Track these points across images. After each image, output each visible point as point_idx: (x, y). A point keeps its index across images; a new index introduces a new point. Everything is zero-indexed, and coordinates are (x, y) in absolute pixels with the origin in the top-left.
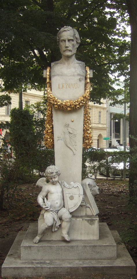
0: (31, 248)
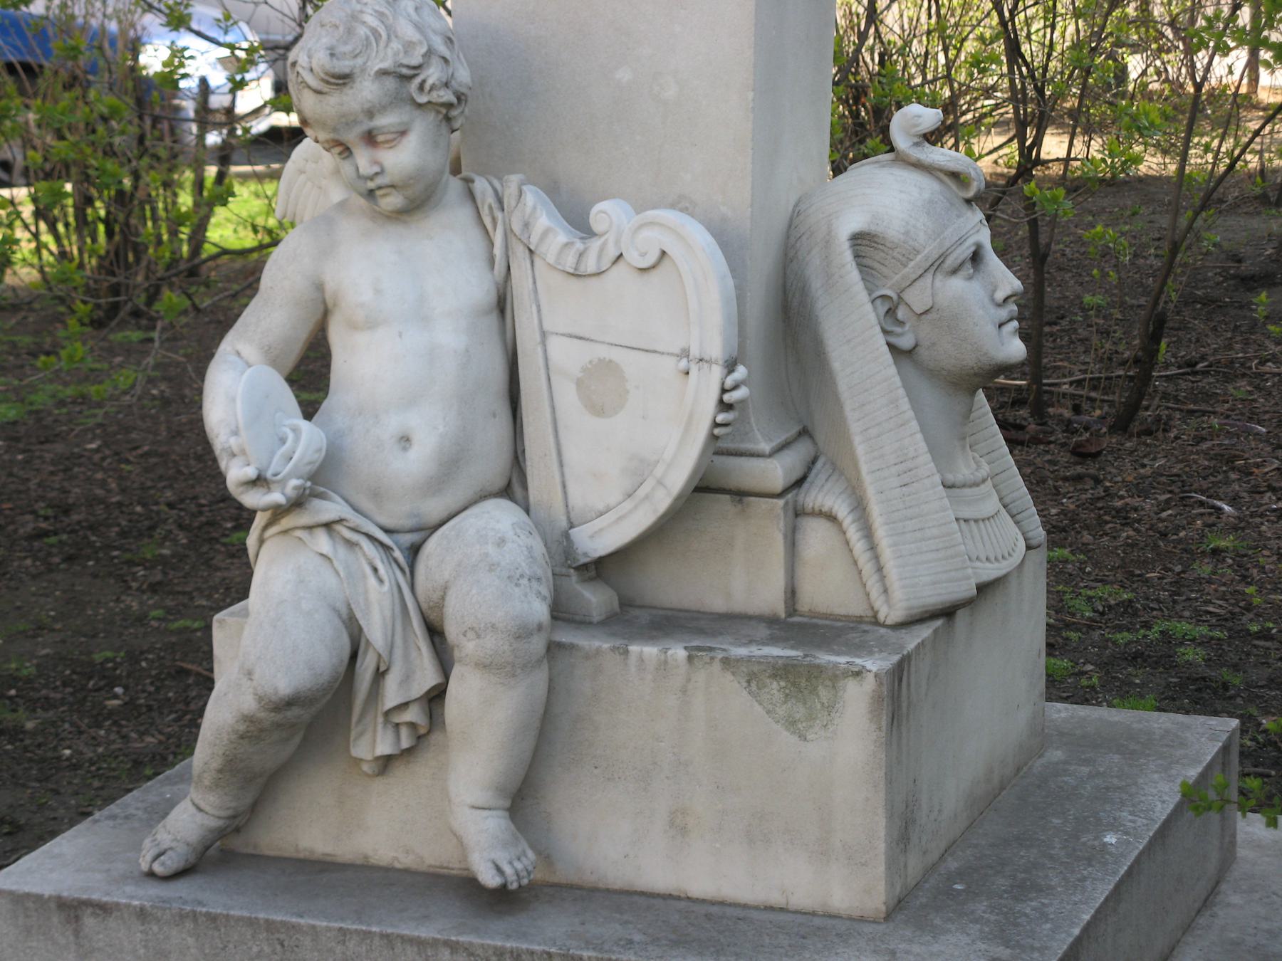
0: (77, 918)
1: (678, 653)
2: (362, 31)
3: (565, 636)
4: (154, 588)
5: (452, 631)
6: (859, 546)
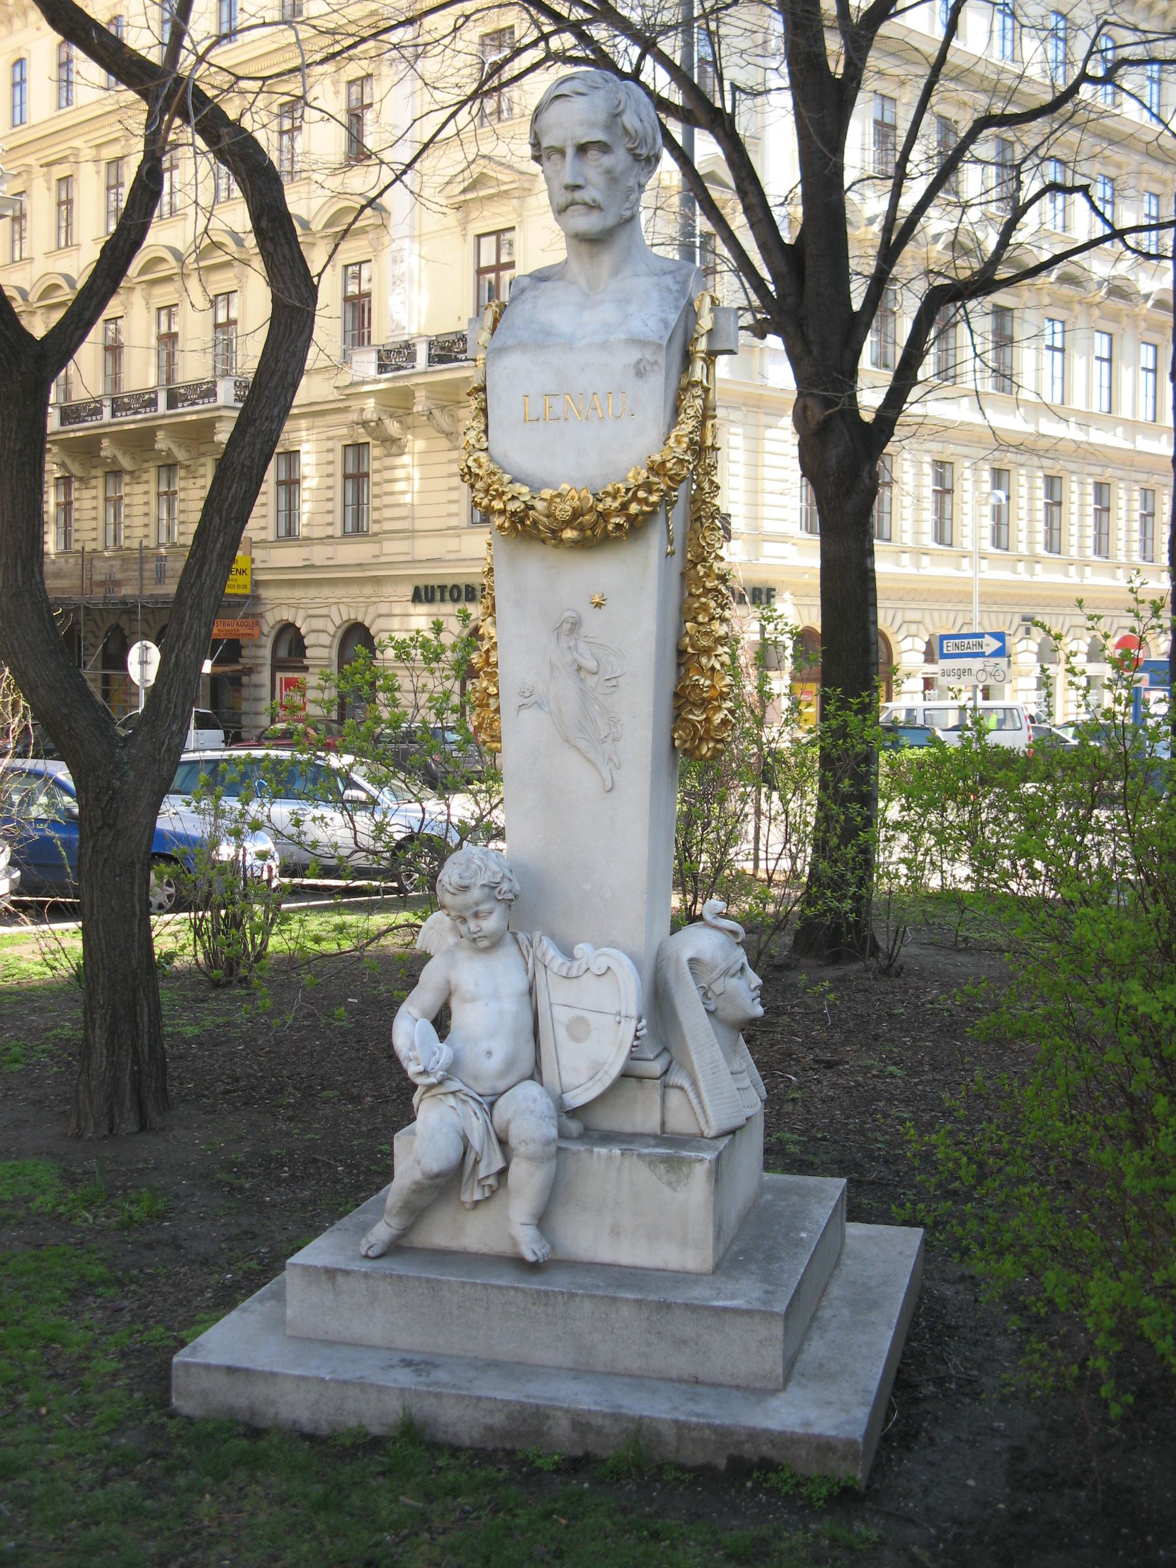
1: (617, 1152)
2: (474, 867)
3: (563, 1144)
4: (291, 1119)
5: (513, 1142)
6: (695, 1101)
